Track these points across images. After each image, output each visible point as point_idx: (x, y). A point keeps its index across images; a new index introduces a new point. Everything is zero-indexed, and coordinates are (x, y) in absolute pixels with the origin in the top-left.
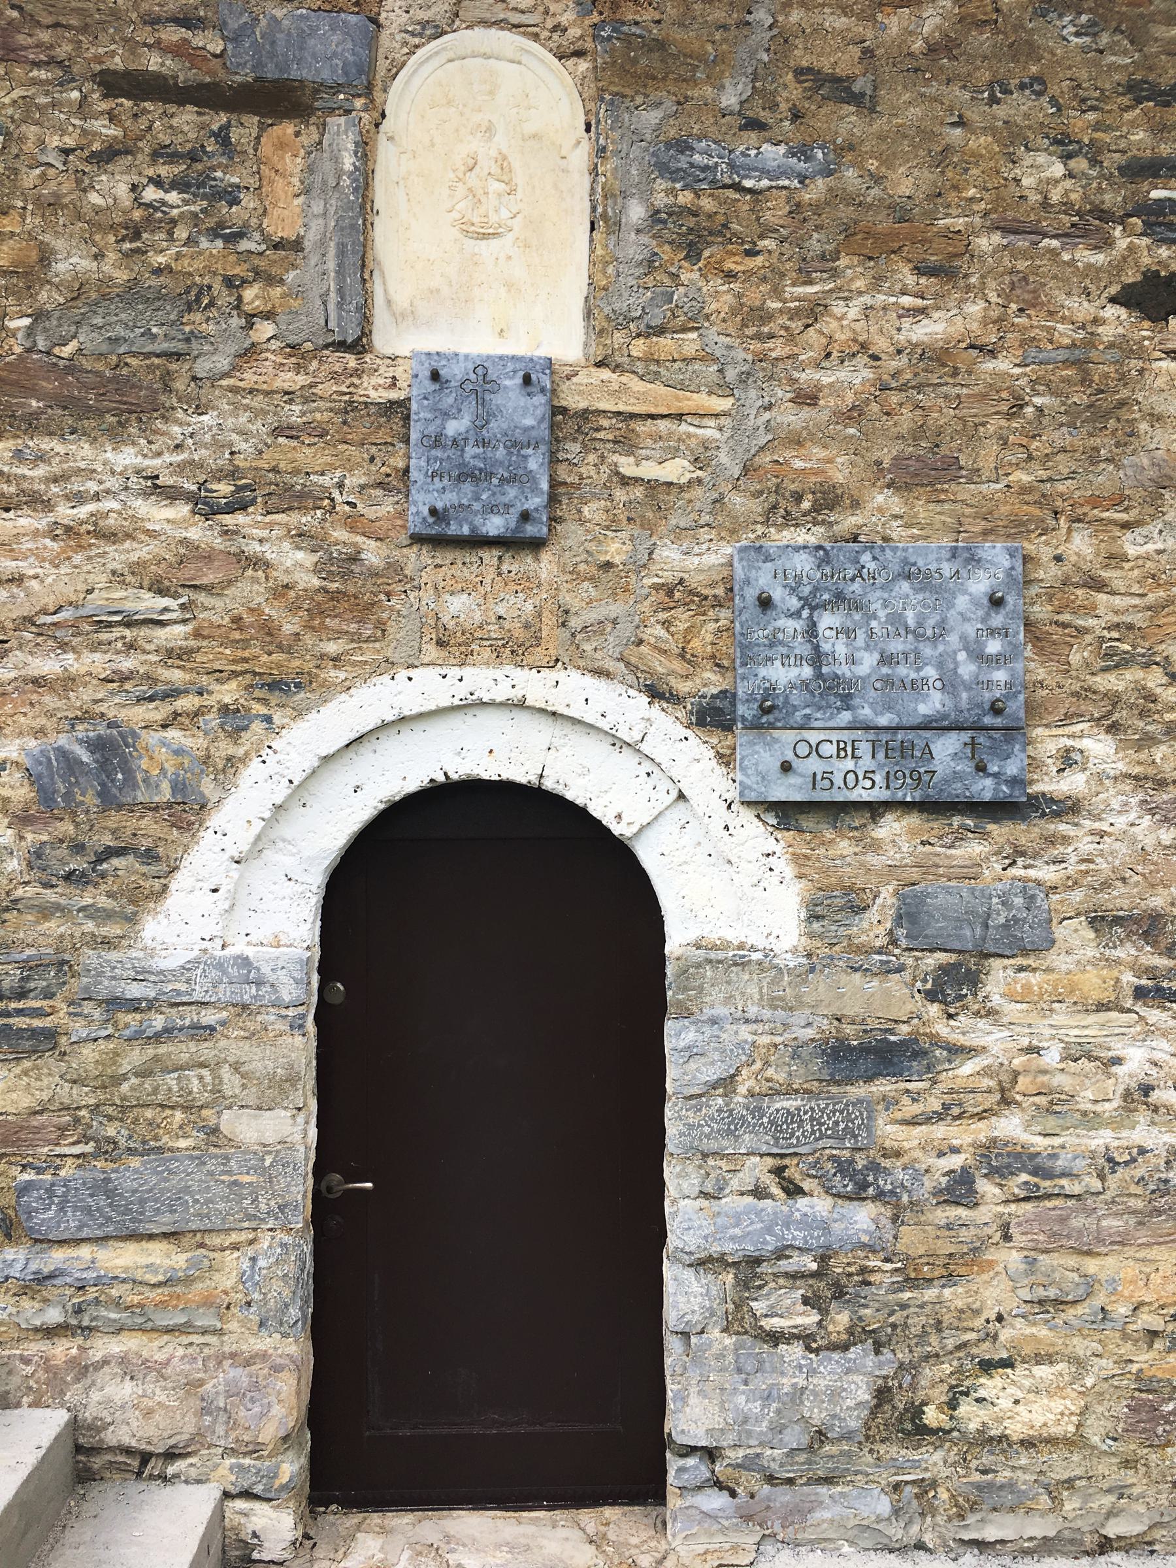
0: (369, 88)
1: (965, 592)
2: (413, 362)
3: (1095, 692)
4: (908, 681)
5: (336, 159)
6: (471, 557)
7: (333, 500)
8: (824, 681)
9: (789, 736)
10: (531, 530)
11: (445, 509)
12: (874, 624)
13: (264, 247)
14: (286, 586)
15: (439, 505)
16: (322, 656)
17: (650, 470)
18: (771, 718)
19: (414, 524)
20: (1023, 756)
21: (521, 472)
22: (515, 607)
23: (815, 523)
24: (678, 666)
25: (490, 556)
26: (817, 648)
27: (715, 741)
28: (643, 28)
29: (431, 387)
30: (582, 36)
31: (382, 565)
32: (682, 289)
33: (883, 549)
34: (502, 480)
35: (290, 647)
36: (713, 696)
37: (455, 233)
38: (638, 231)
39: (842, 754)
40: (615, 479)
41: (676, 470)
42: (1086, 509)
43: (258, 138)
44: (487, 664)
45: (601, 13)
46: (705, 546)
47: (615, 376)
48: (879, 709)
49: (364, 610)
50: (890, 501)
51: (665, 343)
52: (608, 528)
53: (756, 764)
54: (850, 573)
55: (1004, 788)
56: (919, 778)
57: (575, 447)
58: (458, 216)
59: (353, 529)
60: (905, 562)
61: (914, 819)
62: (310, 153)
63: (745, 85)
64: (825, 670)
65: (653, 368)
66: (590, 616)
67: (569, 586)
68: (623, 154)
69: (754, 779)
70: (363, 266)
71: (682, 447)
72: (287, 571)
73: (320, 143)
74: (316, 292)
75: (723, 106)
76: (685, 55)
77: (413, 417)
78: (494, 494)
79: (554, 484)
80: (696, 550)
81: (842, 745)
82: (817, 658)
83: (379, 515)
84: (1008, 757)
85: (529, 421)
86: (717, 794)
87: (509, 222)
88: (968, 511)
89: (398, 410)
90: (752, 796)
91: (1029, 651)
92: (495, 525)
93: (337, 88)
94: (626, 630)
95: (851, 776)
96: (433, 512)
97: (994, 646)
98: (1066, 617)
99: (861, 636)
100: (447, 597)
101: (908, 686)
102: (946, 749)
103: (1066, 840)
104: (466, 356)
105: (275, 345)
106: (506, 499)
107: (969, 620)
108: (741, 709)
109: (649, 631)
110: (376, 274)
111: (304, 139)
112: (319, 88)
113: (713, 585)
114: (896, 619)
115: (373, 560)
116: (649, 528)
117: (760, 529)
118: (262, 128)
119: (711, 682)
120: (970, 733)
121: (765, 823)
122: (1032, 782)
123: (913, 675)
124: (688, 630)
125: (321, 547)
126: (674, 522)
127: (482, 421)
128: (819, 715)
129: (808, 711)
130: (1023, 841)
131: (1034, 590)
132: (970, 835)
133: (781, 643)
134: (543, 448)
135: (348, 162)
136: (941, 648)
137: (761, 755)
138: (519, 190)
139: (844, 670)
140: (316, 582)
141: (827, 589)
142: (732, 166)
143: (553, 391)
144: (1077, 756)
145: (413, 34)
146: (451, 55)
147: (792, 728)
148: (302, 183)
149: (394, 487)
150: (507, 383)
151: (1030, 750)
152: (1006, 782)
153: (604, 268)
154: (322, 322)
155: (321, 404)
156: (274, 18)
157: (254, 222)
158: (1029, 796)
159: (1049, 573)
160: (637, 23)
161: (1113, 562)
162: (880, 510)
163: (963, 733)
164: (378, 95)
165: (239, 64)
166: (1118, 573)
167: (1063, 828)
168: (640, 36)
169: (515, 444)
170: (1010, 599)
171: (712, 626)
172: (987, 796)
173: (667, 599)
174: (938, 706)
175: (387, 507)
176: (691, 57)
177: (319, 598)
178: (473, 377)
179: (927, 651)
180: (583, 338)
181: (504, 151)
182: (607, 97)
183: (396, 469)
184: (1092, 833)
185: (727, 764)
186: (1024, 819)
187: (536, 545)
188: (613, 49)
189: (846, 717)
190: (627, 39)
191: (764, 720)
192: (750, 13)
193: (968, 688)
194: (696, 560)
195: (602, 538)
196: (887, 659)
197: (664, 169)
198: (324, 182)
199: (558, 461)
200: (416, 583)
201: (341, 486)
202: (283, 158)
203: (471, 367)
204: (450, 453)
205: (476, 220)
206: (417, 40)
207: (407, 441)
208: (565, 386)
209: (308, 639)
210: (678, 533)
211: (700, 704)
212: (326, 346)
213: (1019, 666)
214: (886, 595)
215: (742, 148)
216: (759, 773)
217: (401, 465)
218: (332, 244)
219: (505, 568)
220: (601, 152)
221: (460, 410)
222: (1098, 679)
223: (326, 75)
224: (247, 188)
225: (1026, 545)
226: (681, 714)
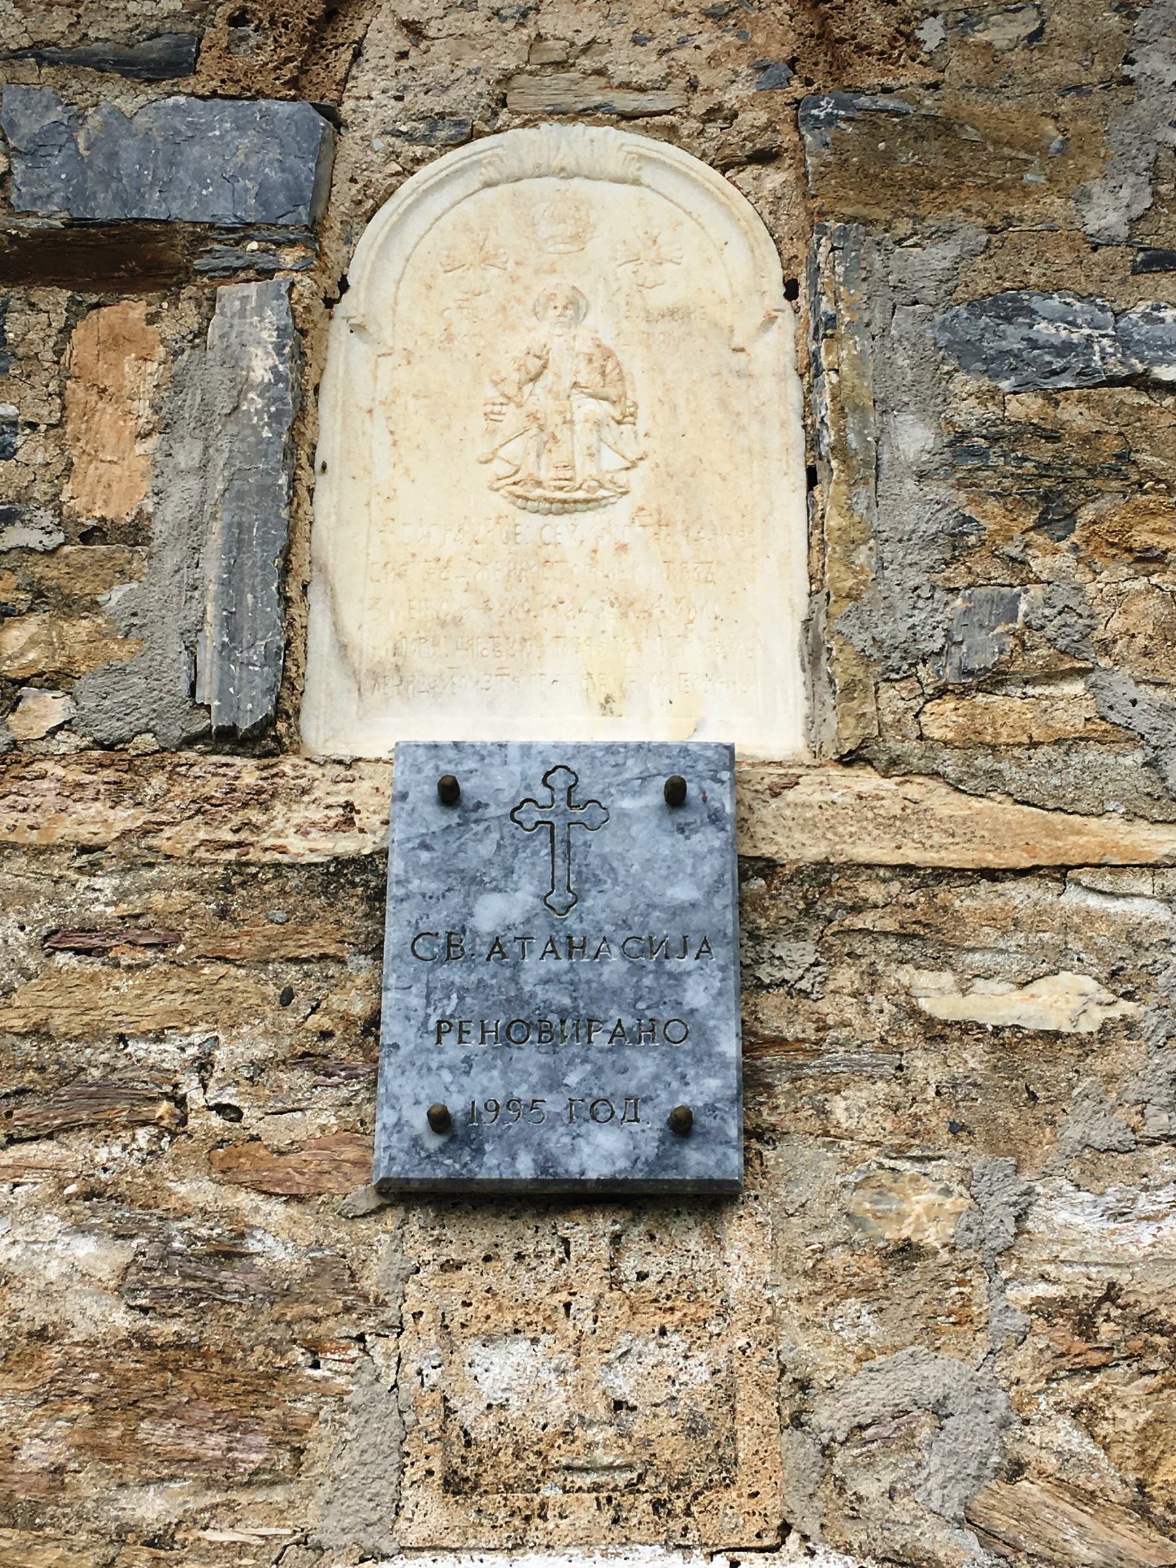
0: (314, 231)
2: (396, 771)
5: (234, 361)
6: (537, 1238)
7: (181, 1102)
10: (697, 1162)
11: (472, 1114)
13: (59, 538)
14: (40, 1335)
15: (456, 1105)
16: (122, 1534)
17: (996, 1004)
19: (389, 1156)
21: (667, 1014)
22: (665, 1373)
25: (588, 1234)
28: (903, 98)
29: (437, 819)
30: (770, 123)
31: (301, 1267)
32: (1036, 590)
34: (619, 1035)
35: (35, 1508)
37: (499, 502)
38: (922, 476)
40: (909, 1028)
41: (1063, 1001)
43: (66, 331)
44: (586, 1543)
45: (808, 82)
47: (890, 784)
49: (245, 1394)
51: (1009, 708)
52: (900, 1152)
57: (801, 953)
58: (507, 469)
59: (227, 1175)
62: (176, 354)
63: (1136, 188)
65: (983, 762)
66: (871, 1395)
67: (804, 1311)
68: (875, 329)
70: (286, 571)
71: (1076, 945)
72: (46, 1294)
73: (201, 333)
74: (173, 625)
75: (1090, 229)
76: (996, 142)
77: (393, 890)
78: (598, 1072)
79: (754, 1043)
80: (1144, 1204)
83: (299, 1134)
85: (683, 892)
87: (622, 478)
89: (357, 880)
92: (601, 1153)
93: (242, 231)
94: (971, 1433)
96: (440, 1121)
100: (472, 1349)
104: (526, 750)
105: (66, 743)
106: (628, 1084)
109: (1038, 1435)
110: (314, 592)
111: (167, 328)
112: (203, 235)
115: (280, 1254)
116: (1010, 1148)
118: (77, 311)
124: (1146, 1433)
125: (142, 1225)
126: (1074, 1132)
127: (565, 895)
134: (721, 954)
135: (261, 365)
138: (642, 413)
140: (122, 1320)
142: (1124, 342)
143: (742, 824)
145: (410, 137)
146: (491, 173)
148: (156, 409)
149: (341, 1065)
150: (627, 804)
153: (848, 553)
154: (183, 687)
155: (167, 871)
156: (118, 112)
157: (41, 490)
160: (887, 90)
164: (330, 243)
165: (35, 198)
168: (897, 113)
169: (650, 946)
173: (1079, 1345)
175: (321, 1114)
176: (1009, 144)
177: (127, 1363)
178: (542, 794)
180: (803, 708)
181: (607, 342)
182: (832, 224)
183: (346, 1019)
187: (712, 1201)
188: (840, 139)
190: (871, 121)
192: (1132, 62)
194: (1146, 1233)
195: (885, 1178)
197: (966, 353)
198: (206, 406)
199: (761, 986)
200: (389, 1314)
201: (204, 1065)
202: (117, 365)
203: (537, 771)
204: (484, 972)
205: (544, 475)
206: (418, 150)
207: (376, 951)
208: (767, 811)
209: (88, 1484)
210: (1092, 1161)
212: (189, 742)
215: (1142, 307)
217: (360, 1008)
218: (216, 526)
219: (629, 1266)
220: (825, 328)
221: (509, 872)
223: (223, 210)
224: (33, 426)
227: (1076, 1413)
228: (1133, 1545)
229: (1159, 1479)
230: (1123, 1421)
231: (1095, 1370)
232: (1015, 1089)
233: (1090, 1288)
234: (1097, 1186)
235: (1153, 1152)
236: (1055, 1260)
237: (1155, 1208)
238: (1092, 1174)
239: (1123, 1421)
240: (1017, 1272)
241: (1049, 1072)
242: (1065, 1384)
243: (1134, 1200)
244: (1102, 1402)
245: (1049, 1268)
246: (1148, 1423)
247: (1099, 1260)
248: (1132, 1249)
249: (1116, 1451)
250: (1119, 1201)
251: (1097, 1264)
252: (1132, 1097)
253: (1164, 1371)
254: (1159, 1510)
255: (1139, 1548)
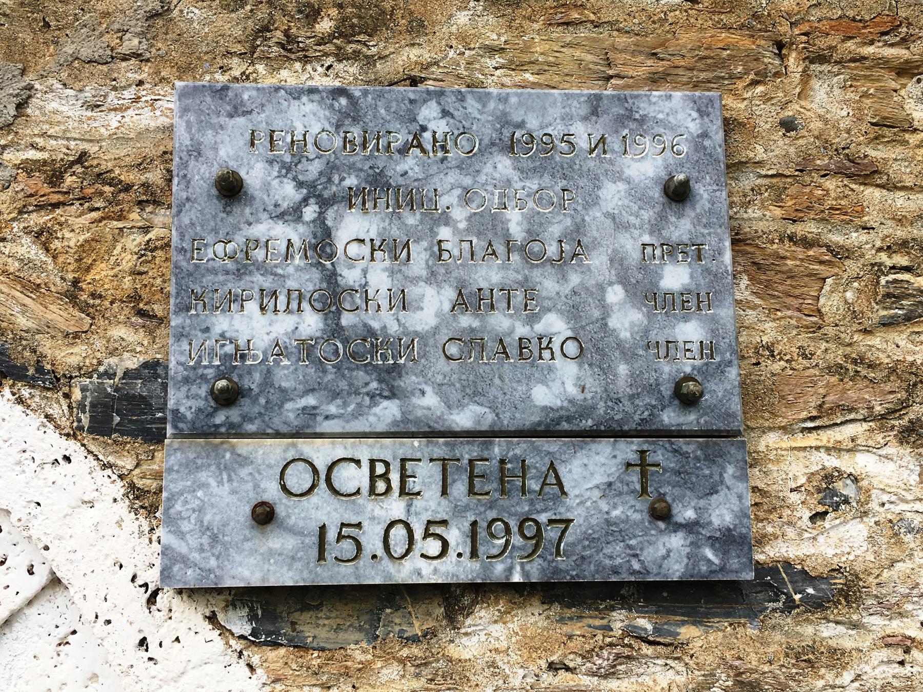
1: (619, 177)
3: (871, 366)
4: (511, 343)
8: (346, 341)
9: (273, 451)
12: (444, 233)
18: (234, 414)
20: (741, 487)
23: (341, 57)
24: (60, 315)
26: (331, 277)
27: (127, 463)
33: (461, 97)
36: (127, 374)
39: (381, 486)
42: (833, 40)
46: (128, 94)
48: (455, 396)
50: (481, 22)
53: (200, 510)
54: (401, 138)
55: (709, 554)
56: (538, 535)
60: (504, 120)
61: (533, 619)
64: (347, 319)
69: (193, 541)
81: (380, 469)
82: (332, 297)
84: (713, 491)
86: (127, 573)
88: (622, 41)
90: (191, 577)
91: (744, 289)
95: (398, 532)
97: (675, 277)
98: (809, 228)
99: (420, 255)
101: (513, 351)
102: (590, 475)
103: (837, 658)
107: (627, 227)
108: (175, 398)
113: (142, 165)
114: (487, 225)
117: (237, 67)
119: (125, 346)
120: (636, 444)
121: (224, 631)
122: (762, 540)
123: (522, 330)
124: (85, 248)
126: (69, 49)
128: (333, 409)
129: (311, 400)
130: (753, 660)
131: (748, 181)
132: (647, 650)
133: (262, 268)
136: (575, 279)
137: (214, 491)
139: (386, 321)
141: (352, 167)
144: (846, 489)
147: (278, 435)
151: (756, 477)
152: (713, 541)
158: (760, 569)
159: (772, 151)
161: (887, 132)
162: (463, 38)
163: (622, 443)
166: (896, 152)
167: (830, 632)
170: (703, 191)
171: (134, 241)
172: (676, 570)
173: (46, 189)
174: (572, 390)
179: (548, 284)
184: (888, 642)
185: (151, 510)
186: (752, 614)
189: (387, 412)
191: (220, 418)
193: (629, 355)
194: (114, 120)
196: (468, 300)
210: (76, 69)
211: (100, 388)
213: (725, 313)
214: (467, 181)
216: (205, 529)
222: (876, 341)
225: (729, 101)
226: (59, 409)
227: (39, 235)
228: (59, 318)
229: (89, 278)
230: (70, 239)
231: (56, 205)
232: (35, 19)
233: (67, 155)
234: (78, 85)
235: (124, 64)
236: (44, 135)
237: (120, 102)
238: (76, 77)
239: (70, 239)
240: (12, 141)
241: (61, 8)
242: (34, 216)
243: (105, 96)
244: (57, 227)
245: (37, 140)
246: (86, 241)
247: (77, 136)
248: (103, 130)
249: (61, 259)
250: (94, 96)
251: (75, 139)
252: (116, 26)
253: (104, 208)
254: (84, 297)
255: (63, 320)
